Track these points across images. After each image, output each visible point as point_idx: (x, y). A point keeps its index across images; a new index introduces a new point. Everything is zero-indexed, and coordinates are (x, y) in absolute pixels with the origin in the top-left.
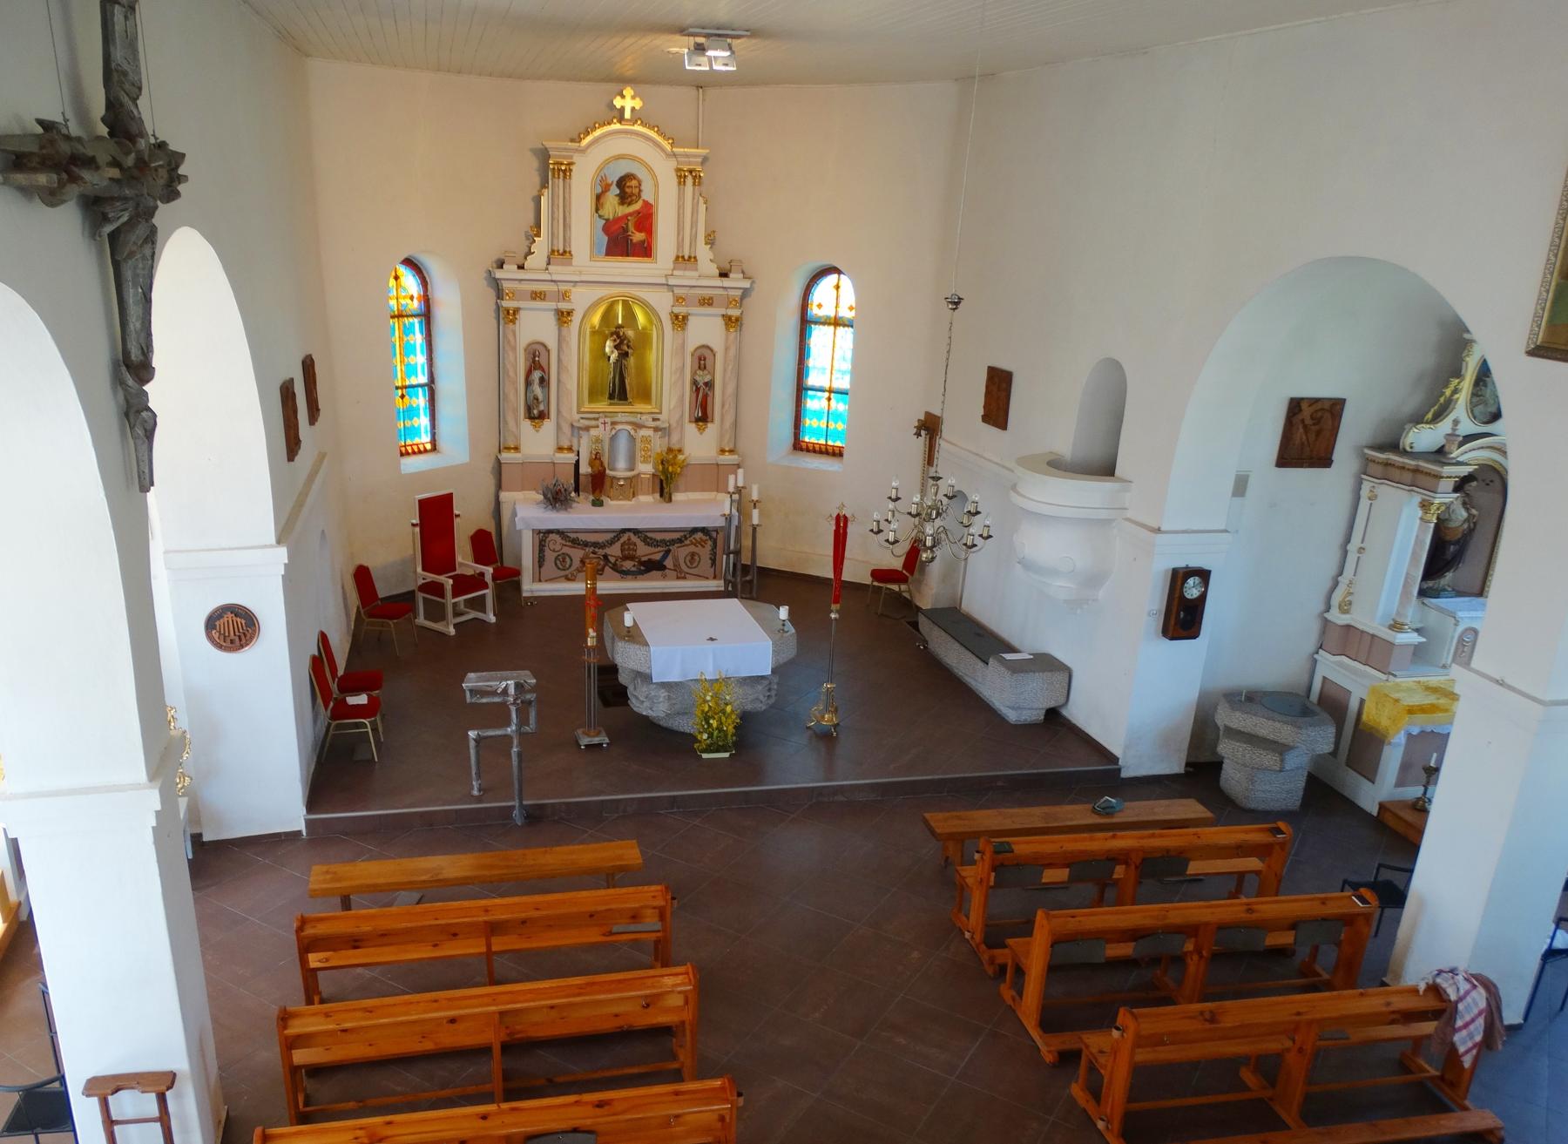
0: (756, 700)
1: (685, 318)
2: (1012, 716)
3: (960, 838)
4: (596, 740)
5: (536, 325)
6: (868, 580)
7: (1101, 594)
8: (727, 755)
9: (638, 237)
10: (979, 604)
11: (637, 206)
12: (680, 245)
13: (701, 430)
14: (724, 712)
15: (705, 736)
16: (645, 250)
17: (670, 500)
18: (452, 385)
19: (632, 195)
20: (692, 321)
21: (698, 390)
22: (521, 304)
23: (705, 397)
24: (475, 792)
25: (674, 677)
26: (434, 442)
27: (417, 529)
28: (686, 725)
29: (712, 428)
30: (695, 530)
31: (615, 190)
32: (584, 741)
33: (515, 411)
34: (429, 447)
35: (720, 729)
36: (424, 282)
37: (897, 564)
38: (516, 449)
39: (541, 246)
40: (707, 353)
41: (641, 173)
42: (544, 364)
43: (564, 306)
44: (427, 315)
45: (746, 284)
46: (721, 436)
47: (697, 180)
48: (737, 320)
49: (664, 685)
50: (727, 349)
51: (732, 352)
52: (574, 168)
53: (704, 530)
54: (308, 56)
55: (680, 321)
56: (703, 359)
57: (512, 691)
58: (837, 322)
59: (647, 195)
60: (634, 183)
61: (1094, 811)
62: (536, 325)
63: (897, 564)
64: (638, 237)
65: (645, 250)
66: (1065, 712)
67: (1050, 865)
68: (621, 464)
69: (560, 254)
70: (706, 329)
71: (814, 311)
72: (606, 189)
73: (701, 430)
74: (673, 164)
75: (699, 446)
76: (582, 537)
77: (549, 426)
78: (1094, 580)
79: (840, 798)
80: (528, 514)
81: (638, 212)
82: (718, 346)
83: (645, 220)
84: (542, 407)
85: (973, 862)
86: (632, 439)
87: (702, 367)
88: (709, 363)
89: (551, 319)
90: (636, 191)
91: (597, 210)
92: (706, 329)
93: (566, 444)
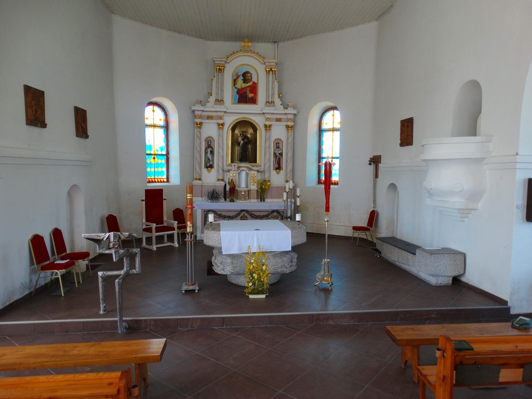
0: (286, 266)
1: (270, 126)
2: (433, 281)
3: (416, 344)
4: (191, 288)
5: (210, 129)
6: (349, 233)
7: (480, 205)
8: (264, 296)
9: (251, 95)
10: (405, 233)
11: (250, 84)
12: (268, 97)
13: (278, 173)
14: (262, 270)
15: (251, 284)
16: (253, 101)
17: (264, 201)
18: (175, 154)
19: (248, 79)
20: (273, 128)
21: (276, 156)
22: (203, 121)
23: (279, 159)
24: (102, 312)
25: (235, 251)
26: (168, 178)
27: (144, 203)
28: (243, 281)
29: (282, 172)
30: (273, 211)
31: (241, 78)
32: (185, 288)
33: (200, 164)
34: (165, 180)
35: (259, 279)
36: (166, 115)
37: (364, 223)
38: (200, 179)
39: (212, 99)
40: (279, 141)
41: (252, 71)
42: (212, 145)
43: (220, 122)
44: (166, 127)
45: (295, 112)
46: (286, 175)
47: (274, 72)
48: (292, 127)
49: (230, 256)
50: (288, 139)
51: (290, 140)
52: (225, 69)
53: (277, 211)
54: (113, 13)
55: (268, 128)
56: (278, 145)
57: (112, 239)
58: (334, 130)
59: (254, 79)
60: (249, 75)
61: (513, 327)
62: (210, 129)
63: (364, 223)
64: (251, 95)
65: (253, 101)
66: (464, 279)
67: (505, 365)
68: (243, 185)
69: (220, 101)
70: (279, 132)
71: (324, 127)
72: (238, 77)
73: (278, 173)
74: (264, 66)
75: (277, 179)
76: (224, 214)
77: (214, 171)
78: (475, 196)
79: (331, 322)
80: (201, 203)
81: (251, 86)
82: (284, 139)
83: (254, 88)
84: (211, 163)
85: (434, 363)
86: (247, 174)
87: (278, 147)
88: (280, 145)
89: (215, 127)
90: (250, 78)
91: (234, 85)
92: (279, 132)
93: (221, 178)
